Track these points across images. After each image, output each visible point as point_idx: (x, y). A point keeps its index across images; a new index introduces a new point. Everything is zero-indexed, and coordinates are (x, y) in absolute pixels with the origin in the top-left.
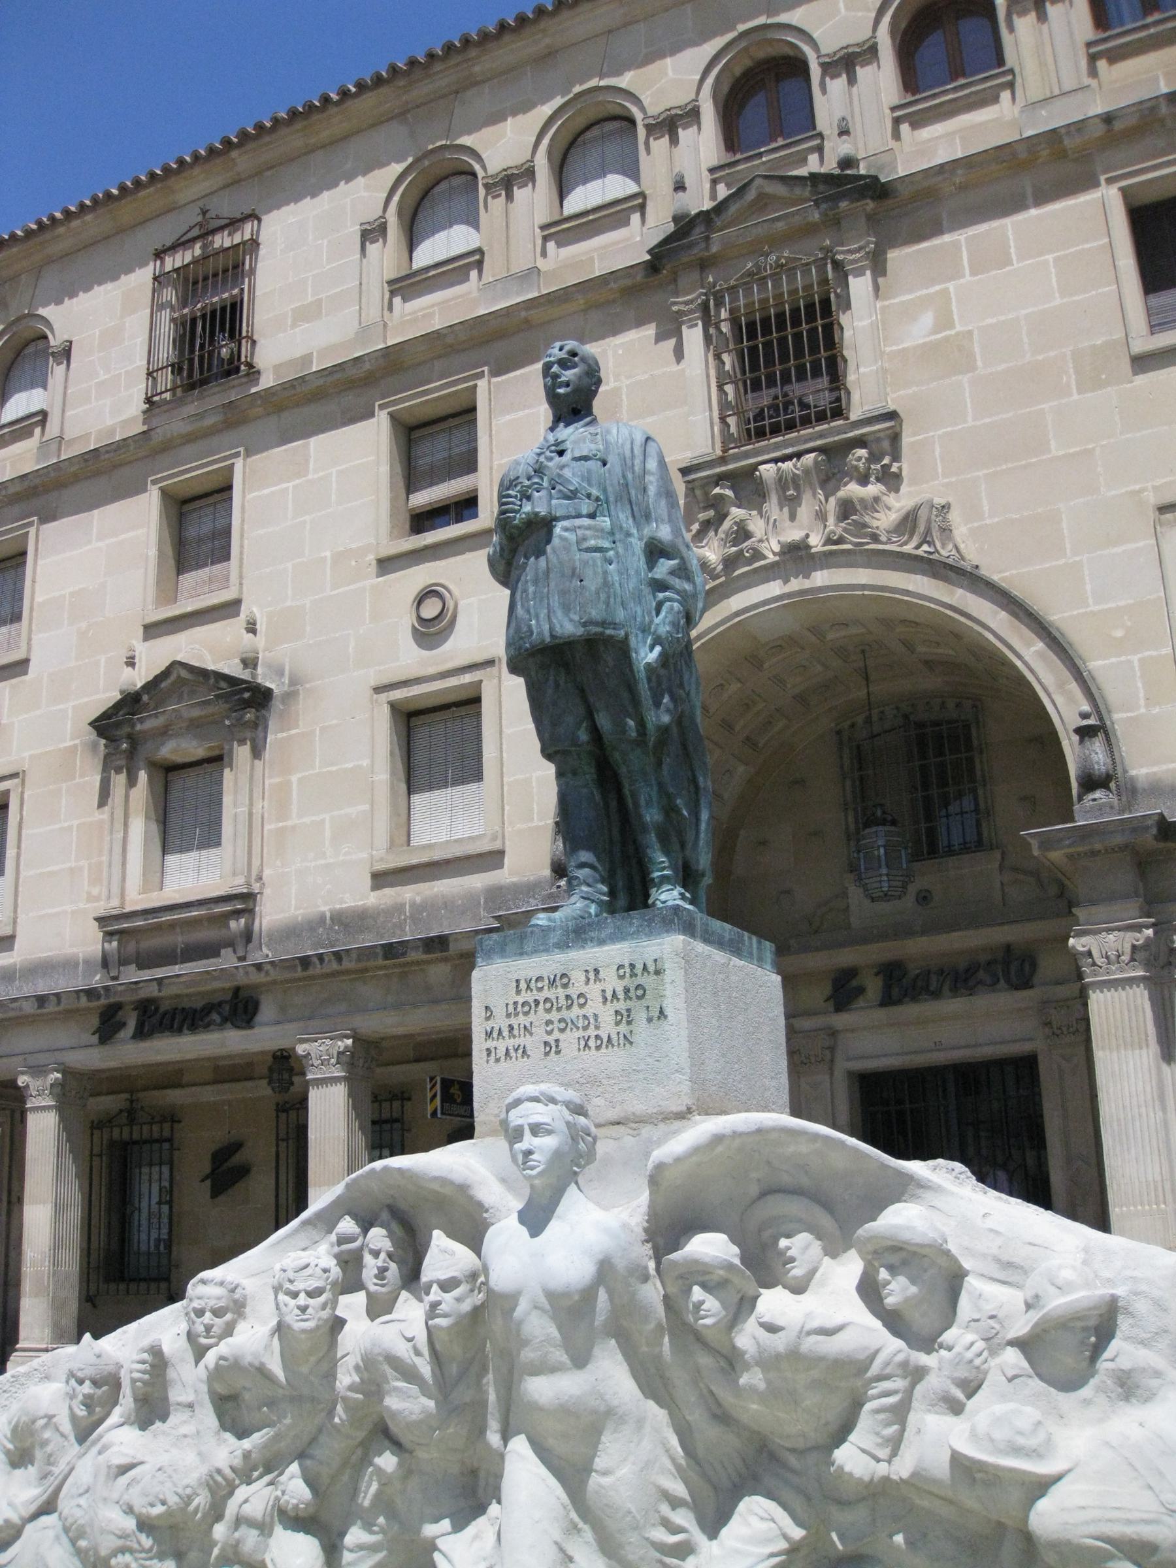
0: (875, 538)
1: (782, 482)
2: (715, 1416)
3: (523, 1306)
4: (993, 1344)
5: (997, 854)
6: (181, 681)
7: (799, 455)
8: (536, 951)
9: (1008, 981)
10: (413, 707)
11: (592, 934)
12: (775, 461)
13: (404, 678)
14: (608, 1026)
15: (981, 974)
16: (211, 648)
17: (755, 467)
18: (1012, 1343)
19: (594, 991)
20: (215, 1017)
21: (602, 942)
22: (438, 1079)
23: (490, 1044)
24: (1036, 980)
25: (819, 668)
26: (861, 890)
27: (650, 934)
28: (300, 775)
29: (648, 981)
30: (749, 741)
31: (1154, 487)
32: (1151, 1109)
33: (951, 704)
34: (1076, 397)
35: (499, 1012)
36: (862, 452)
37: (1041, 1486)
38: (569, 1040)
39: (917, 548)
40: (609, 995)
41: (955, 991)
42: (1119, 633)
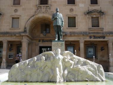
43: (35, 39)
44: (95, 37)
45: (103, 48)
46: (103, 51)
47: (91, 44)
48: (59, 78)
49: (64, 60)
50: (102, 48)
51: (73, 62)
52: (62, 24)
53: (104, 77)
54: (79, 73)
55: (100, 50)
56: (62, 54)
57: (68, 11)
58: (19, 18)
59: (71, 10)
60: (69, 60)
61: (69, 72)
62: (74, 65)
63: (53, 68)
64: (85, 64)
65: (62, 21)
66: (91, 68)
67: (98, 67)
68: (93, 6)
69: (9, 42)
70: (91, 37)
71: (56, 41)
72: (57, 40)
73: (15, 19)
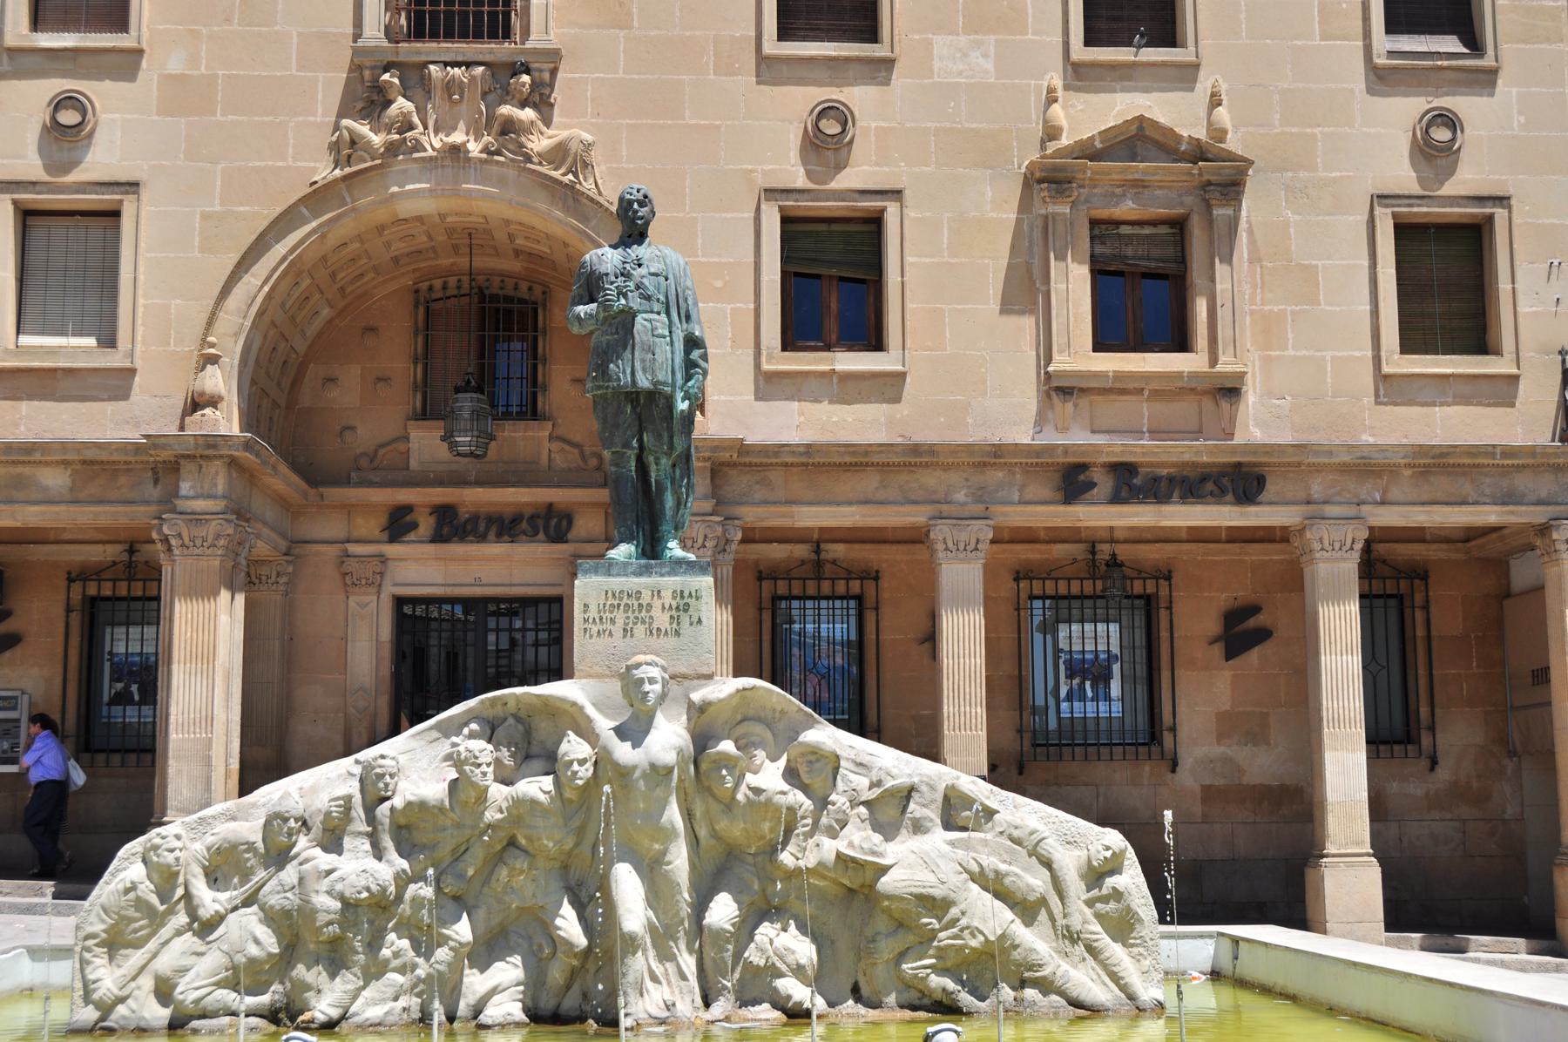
0: (528, 159)
1: (450, 86)
3: (637, 774)
4: (854, 803)
5: (550, 424)
7: (468, 65)
9: (546, 533)
15: (524, 525)
17: (425, 64)
18: (863, 803)
24: (570, 536)
29: (692, 602)
30: (342, 289)
33: (524, 286)
36: (526, 78)
37: (884, 870)
38: (640, 630)
39: (564, 174)
41: (499, 537)
42: (719, 284)
45: (1252, 623)
46: (1253, 656)
47: (1093, 563)
55: (1218, 650)
59: (827, 140)
68: (1038, 335)
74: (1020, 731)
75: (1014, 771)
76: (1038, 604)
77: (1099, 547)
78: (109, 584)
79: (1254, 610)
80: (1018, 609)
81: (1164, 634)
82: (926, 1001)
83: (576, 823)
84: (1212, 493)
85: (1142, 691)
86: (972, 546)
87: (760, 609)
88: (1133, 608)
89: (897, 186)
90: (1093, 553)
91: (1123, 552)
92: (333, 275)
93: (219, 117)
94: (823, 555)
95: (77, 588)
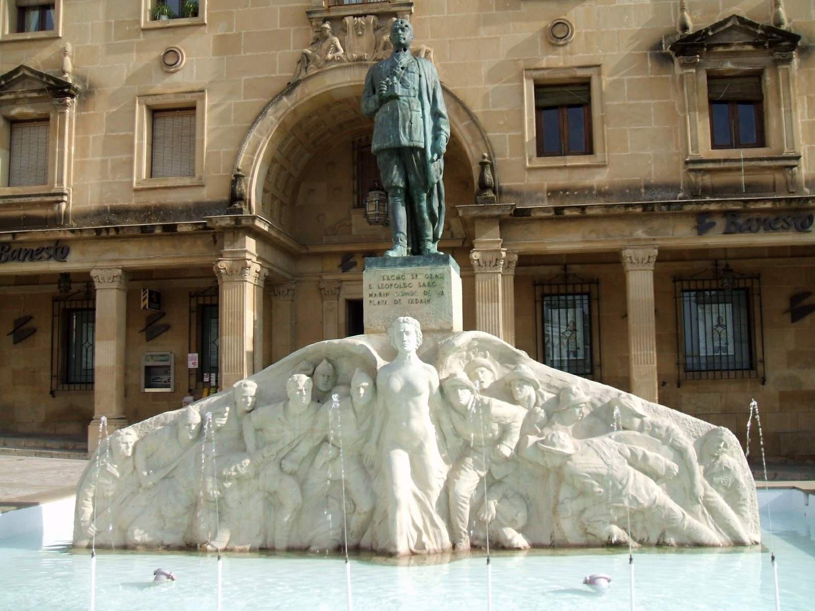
1: (357, 27)
2: (455, 435)
6: (24, 76)
7: (365, 15)
8: (391, 266)
10: (156, 108)
11: (415, 262)
12: (354, 16)
13: (155, 93)
14: (420, 296)
16: (38, 58)
17: (343, 17)
19: (415, 283)
20: (44, 254)
21: (418, 265)
22: (147, 290)
23: (371, 299)
25: (353, 113)
26: (366, 220)
27: (438, 264)
28: (94, 135)
30: (314, 143)
31: (524, 60)
32: (648, 339)
34: (494, 12)
35: (375, 287)
40: (422, 284)
43: (313, 249)
44: (734, 220)
45: (806, 302)
48: (408, 521)
49: (445, 393)
50: (795, 299)
51: (514, 414)
52: (436, 138)
53: (749, 515)
54: (565, 493)
55: (788, 317)
56: (432, 356)
57: (579, 30)
58: (190, 109)
60: (486, 399)
61: (490, 483)
62: (523, 435)
63: (370, 451)
64: (602, 420)
65: (436, 115)
66: (651, 454)
67: (708, 449)
69: (134, 278)
70: (703, 222)
71: (396, 262)
72: (401, 250)
73: (172, 116)
74: (678, 364)
75: (675, 385)
76: (686, 294)
77: (719, 262)
78: (208, 298)
79: (807, 294)
80: (675, 298)
81: (757, 309)
82: (598, 541)
83: (364, 428)
84: (782, 227)
85: (745, 346)
86: (645, 261)
87: (536, 302)
88: (739, 295)
89: (598, 63)
90: (716, 265)
91: (732, 264)
92: (307, 135)
93: (242, 54)
94: (569, 272)
95: (194, 300)
